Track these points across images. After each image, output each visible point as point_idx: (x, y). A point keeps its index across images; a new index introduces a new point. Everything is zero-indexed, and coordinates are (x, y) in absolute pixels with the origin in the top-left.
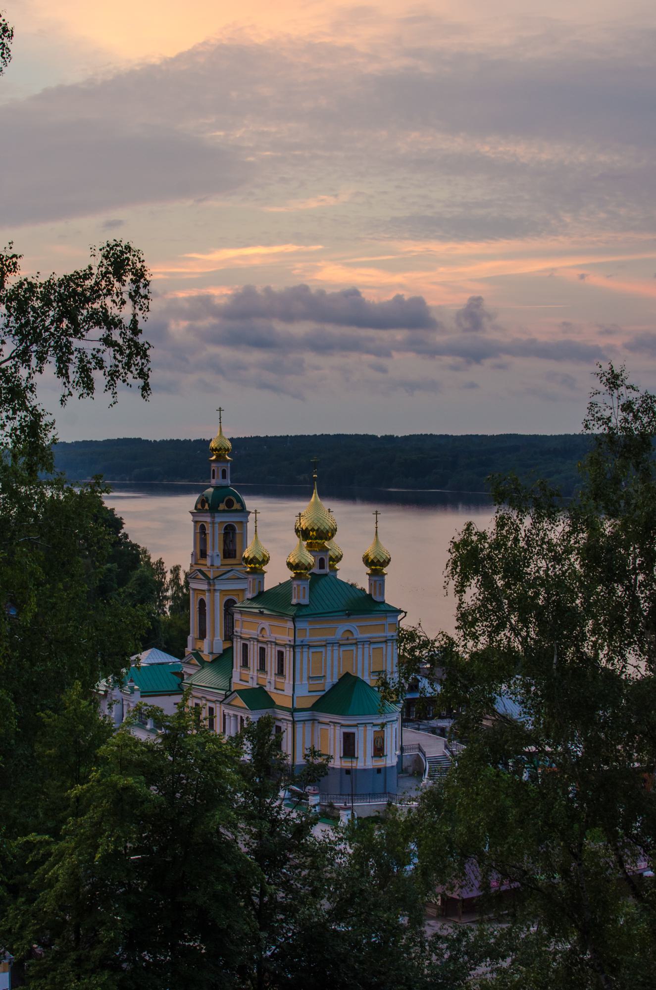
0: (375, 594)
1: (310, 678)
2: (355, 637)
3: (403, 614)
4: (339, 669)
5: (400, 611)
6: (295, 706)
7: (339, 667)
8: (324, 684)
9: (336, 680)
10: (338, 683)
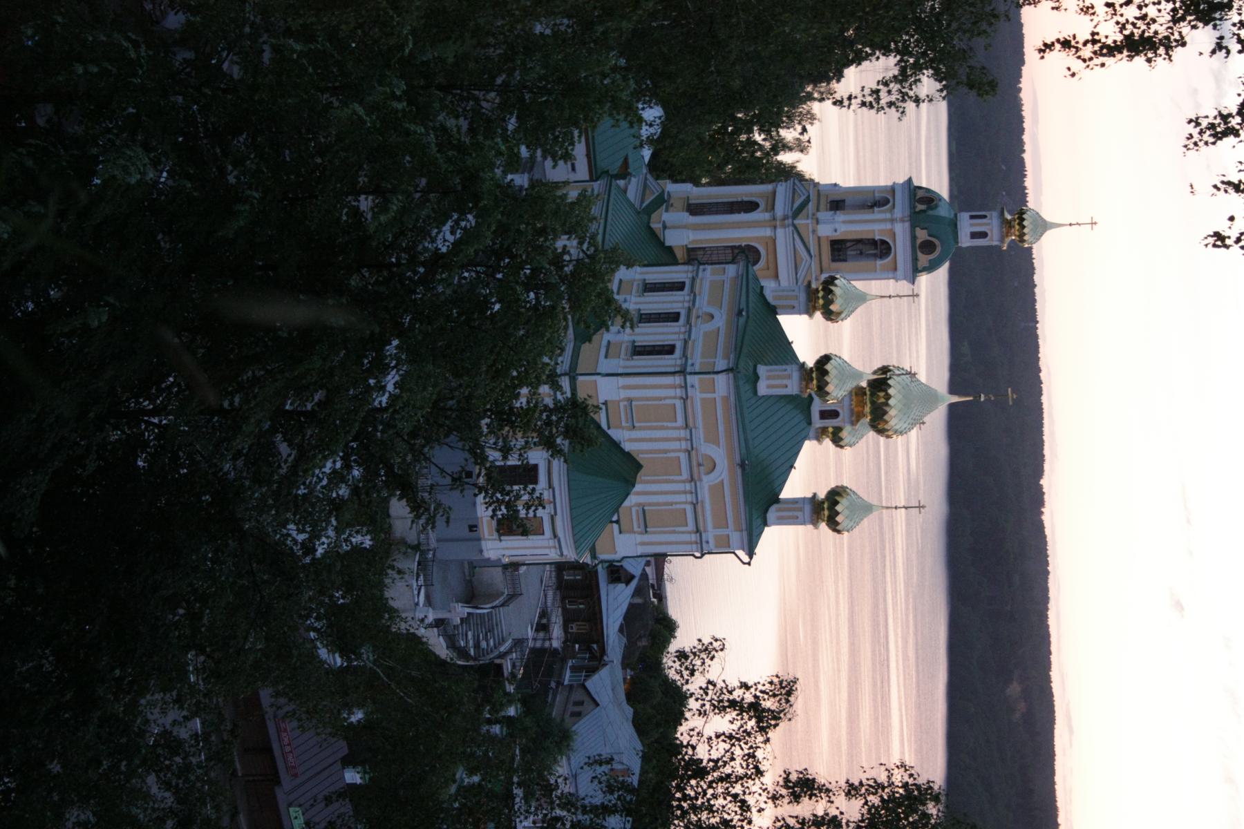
0: (779, 510)
1: (630, 400)
2: (705, 478)
3: (746, 559)
4: (643, 452)
5: (751, 554)
6: (581, 378)
7: (650, 452)
8: (621, 427)
9: (627, 447)
10: (622, 450)
